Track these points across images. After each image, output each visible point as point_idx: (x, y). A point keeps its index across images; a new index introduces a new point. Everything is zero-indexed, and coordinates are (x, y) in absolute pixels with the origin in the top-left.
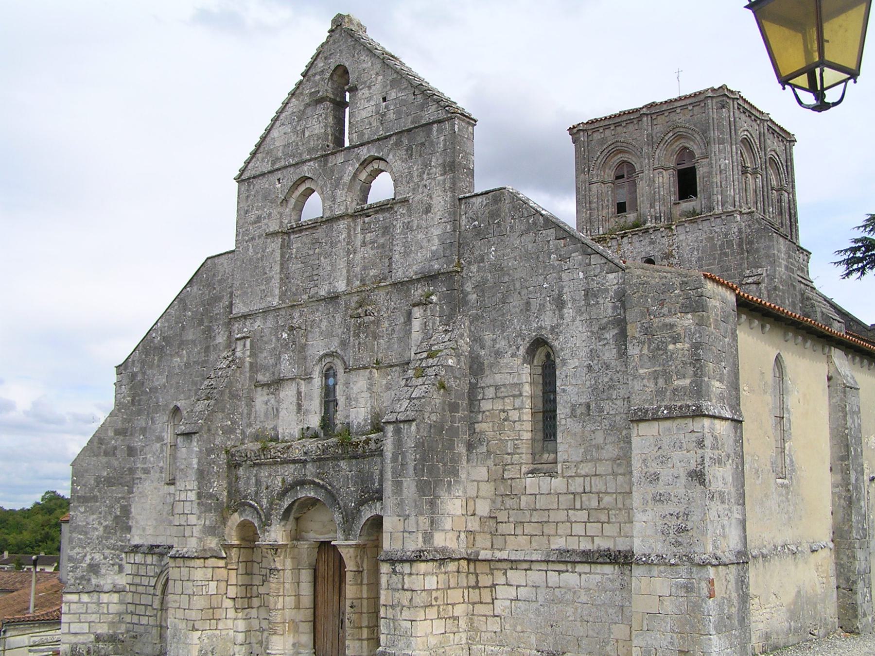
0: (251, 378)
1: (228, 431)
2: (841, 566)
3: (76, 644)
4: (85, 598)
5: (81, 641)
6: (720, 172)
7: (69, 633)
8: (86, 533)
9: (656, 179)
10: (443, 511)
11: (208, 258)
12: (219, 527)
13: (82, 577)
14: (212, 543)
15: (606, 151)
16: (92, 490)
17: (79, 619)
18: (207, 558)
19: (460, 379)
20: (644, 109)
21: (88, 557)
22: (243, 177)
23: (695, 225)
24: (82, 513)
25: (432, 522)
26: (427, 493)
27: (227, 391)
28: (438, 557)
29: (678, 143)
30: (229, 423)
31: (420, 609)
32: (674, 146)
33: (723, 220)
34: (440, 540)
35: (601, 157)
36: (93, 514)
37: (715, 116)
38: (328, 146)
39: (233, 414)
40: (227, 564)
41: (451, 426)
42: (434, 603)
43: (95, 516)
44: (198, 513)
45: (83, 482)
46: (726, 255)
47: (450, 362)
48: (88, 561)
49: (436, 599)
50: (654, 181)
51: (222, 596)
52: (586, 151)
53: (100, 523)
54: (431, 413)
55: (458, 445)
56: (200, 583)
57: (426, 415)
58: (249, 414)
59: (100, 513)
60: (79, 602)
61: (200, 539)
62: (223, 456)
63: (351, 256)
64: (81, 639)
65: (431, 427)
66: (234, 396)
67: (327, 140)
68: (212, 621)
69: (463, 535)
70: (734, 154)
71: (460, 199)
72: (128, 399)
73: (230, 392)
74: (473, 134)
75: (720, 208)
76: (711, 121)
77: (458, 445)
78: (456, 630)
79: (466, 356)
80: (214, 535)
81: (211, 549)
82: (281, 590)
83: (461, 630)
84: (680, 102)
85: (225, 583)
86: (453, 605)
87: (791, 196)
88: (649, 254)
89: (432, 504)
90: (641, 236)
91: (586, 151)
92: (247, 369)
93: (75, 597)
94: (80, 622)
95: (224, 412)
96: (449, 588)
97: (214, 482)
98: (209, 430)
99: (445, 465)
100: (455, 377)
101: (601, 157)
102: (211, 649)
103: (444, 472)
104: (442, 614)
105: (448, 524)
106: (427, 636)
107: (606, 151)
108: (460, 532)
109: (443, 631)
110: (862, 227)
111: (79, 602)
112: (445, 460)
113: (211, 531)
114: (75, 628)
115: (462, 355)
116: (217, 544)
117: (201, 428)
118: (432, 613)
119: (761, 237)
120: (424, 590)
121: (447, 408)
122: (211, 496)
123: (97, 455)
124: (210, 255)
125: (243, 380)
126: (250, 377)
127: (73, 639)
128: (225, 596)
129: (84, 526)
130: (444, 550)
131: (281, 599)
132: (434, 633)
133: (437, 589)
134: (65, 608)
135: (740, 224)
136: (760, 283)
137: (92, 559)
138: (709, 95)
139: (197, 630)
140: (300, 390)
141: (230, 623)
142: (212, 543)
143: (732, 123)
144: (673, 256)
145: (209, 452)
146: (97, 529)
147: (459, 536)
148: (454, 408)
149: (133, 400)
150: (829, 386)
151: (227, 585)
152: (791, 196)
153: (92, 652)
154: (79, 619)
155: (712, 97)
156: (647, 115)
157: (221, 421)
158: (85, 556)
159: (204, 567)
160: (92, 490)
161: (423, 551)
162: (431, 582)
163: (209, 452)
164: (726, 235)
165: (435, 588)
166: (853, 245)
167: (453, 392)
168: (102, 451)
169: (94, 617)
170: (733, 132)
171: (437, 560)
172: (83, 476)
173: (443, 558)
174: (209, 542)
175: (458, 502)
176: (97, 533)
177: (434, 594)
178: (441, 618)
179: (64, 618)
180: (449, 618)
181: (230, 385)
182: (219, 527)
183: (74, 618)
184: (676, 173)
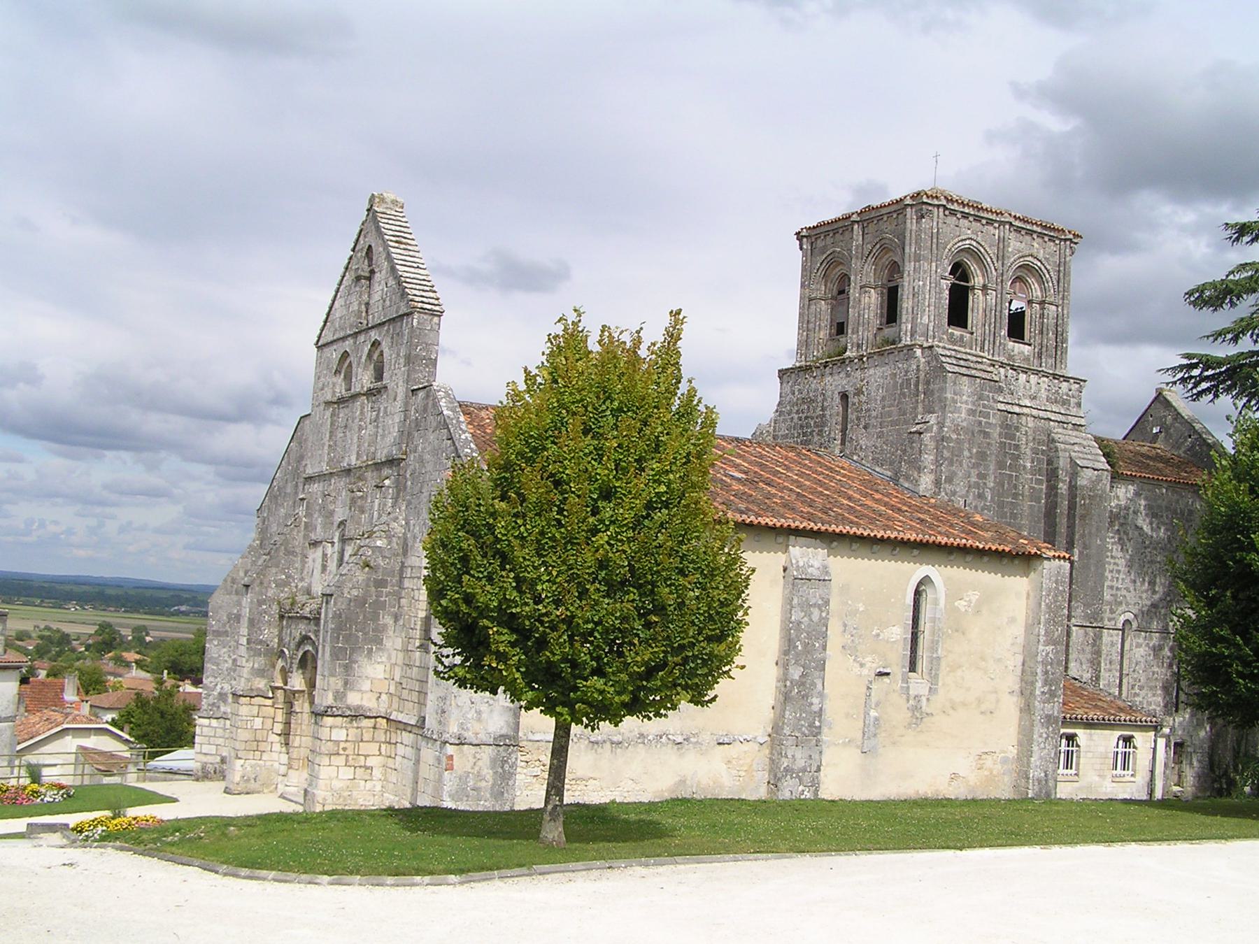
0: (306, 536)
1: (280, 584)
2: (773, 760)
3: (206, 763)
4: (214, 723)
5: (210, 761)
6: (914, 295)
7: (201, 753)
8: (218, 665)
9: (863, 299)
10: (360, 674)
11: (301, 418)
12: (268, 670)
13: (214, 704)
14: (261, 684)
15: (826, 262)
16: (224, 625)
17: (209, 741)
18: (253, 697)
19: (390, 558)
20: (854, 216)
21: (219, 687)
22: (319, 344)
23: (883, 358)
24: (215, 646)
25: (346, 683)
26: (341, 657)
27: (283, 548)
28: (348, 713)
29: (886, 257)
30: (284, 577)
31: (325, 756)
32: (884, 260)
33: (895, 356)
34: (353, 699)
35: (821, 269)
36: (224, 647)
37: (914, 228)
38: (361, 323)
39: (288, 568)
40: (274, 703)
41: (376, 600)
42: (341, 752)
43: (225, 650)
44: (246, 656)
45: (217, 618)
46: (904, 395)
47: (379, 543)
48: (219, 690)
49: (344, 749)
50: (860, 301)
51: (268, 731)
52: (809, 261)
53: (230, 657)
54: (351, 589)
55: (383, 617)
56: (245, 718)
57: (346, 591)
58: (302, 570)
59: (230, 647)
60: (209, 726)
61: (248, 680)
62: (275, 607)
63: (363, 432)
64: (209, 759)
65: (350, 601)
66: (289, 553)
67: (360, 318)
68: (256, 752)
69: (384, 697)
70: (933, 272)
71: (413, 391)
72: (257, 542)
73: (285, 549)
74: (439, 324)
75: (908, 339)
76: (908, 234)
77: (383, 617)
78: (367, 777)
79: (399, 537)
80: (263, 676)
81: (258, 689)
82: (299, 730)
83: (374, 778)
84: (886, 209)
85: (272, 720)
86: (366, 756)
87: (1060, 309)
88: (844, 388)
89: (348, 668)
90: (840, 367)
91: (809, 261)
92: (303, 529)
93: (206, 722)
94: (209, 744)
95: (278, 567)
96: (362, 741)
97: (265, 630)
98: (261, 583)
99: (365, 634)
100: (384, 557)
101: (821, 269)
102: (254, 776)
103: (364, 640)
104: (351, 762)
105: (366, 686)
106: (331, 779)
107: (826, 262)
108: (380, 693)
109: (352, 777)
110: (1211, 336)
111: (209, 726)
112: (367, 630)
113: (260, 673)
114: (206, 749)
115: (394, 536)
116: (266, 685)
117: (253, 581)
118: (340, 760)
119: (936, 377)
120: (330, 740)
121: (372, 584)
122: (261, 642)
123: (230, 594)
124: (303, 415)
125: (298, 539)
126: (305, 535)
127: (205, 759)
128: (270, 732)
129: (216, 658)
130: (359, 707)
131: (298, 738)
132: (340, 777)
133: (347, 741)
134: (198, 730)
135: (919, 361)
136: (922, 433)
137: (222, 688)
138: (907, 203)
139: (240, 758)
140: (326, 552)
141: (275, 756)
142: (261, 684)
143: (935, 236)
144: (863, 393)
145: (260, 603)
146: (226, 661)
147: (380, 697)
148: (380, 584)
149: (261, 544)
150: (784, 577)
151: (274, 722)
152: (1060, 309)
153: (218, 771)
154: (209, 741)
155: (912, 206)
156: (858, 222)
157: (274, 574)
158: (217, 685)
159: (250, 704)
160: (224, 625)
161: (332, 707)
162: (339, 735)
163: (260, 603)
164: (907, 372)
165: (344, 739)
166: (1185, 362)
167: (381, 570)
168: (234, 589)
169: (220, 741)
170: (934, 246)
171: (347, 717)
172: (217, 612)
173: (356, 715)
174: (256, 683)
175: (380, 668)
176: (226, 665)
177: (342, 745)
178: (350, 766)
179: (197, 739)
180: (360, 767)
181: (286, 542)
182: (268, 670)
183: (205, 740)
184: (885, 291)
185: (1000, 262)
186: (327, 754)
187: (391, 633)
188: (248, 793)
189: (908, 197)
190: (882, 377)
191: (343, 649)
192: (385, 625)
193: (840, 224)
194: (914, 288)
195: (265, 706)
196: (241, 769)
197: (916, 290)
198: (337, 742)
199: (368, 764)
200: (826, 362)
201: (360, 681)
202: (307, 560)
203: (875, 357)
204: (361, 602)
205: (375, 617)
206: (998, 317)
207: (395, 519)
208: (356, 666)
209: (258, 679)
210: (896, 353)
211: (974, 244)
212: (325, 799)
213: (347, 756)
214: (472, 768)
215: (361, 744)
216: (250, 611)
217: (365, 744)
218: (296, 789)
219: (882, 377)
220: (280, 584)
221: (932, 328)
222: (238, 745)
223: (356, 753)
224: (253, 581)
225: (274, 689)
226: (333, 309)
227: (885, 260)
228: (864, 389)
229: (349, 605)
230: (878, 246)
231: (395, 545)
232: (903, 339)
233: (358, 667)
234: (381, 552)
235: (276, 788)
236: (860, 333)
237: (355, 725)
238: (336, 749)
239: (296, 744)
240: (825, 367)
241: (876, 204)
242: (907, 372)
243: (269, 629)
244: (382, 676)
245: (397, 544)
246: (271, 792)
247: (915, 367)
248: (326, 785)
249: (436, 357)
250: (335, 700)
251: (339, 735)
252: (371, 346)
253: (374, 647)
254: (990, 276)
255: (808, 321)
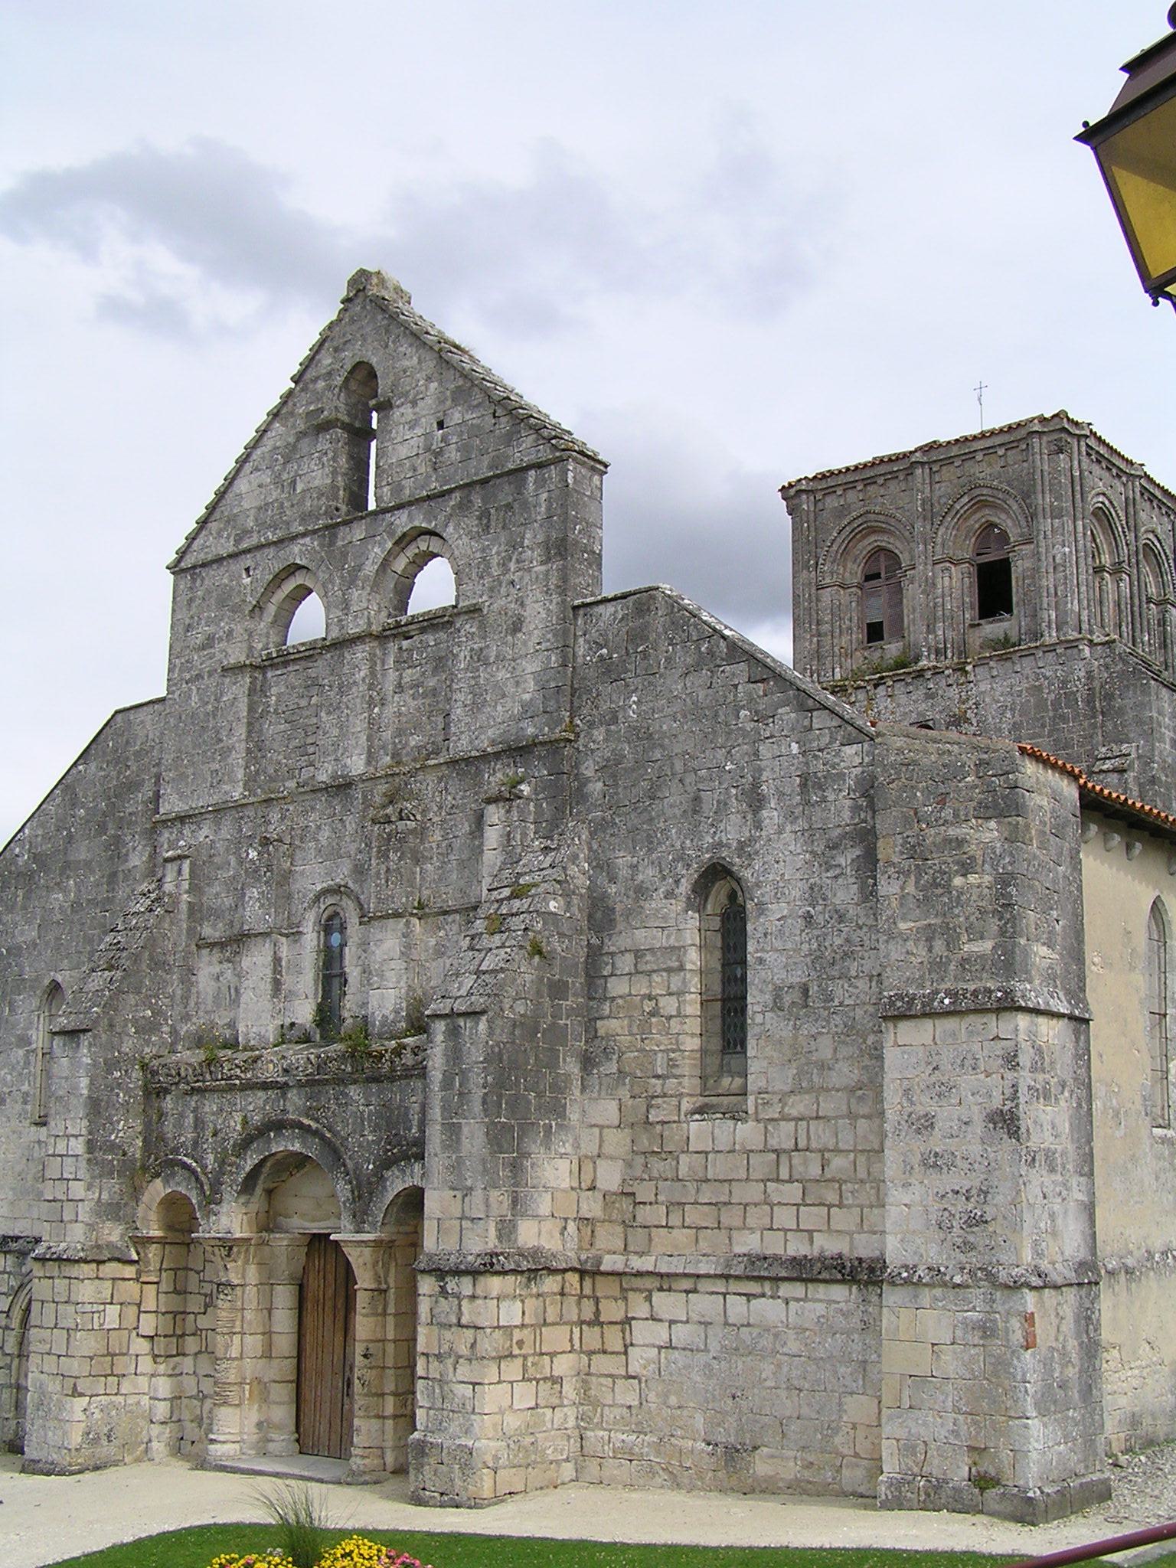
6: (1055, 568)
11: (117, 712)
12: (126, 1204)
19: (570, 937)
20: (917, 454)
25: (515, 1202)
26: (505, 1146)
28: (525, 1266)
29: (978, 515)
34: (528, 1234)
38: (337, 509)
39: (157, 996)
40: (139, 1273)
42: (516, 1351)
46: (1064, 718)
47: (553, 906)
49: (520, 1344)
51: (130, 1332)
52: (812, 529)
54: (515, 1000)
56: (88, 1308)
58: (186, 998)
61: (91, 1227)
62: (136, 1074)
63: (376, 710)
65: (514, 1026)
66: (157, 964)
71: (575, 608)
73: (151, 959)
76: (1038, 476)
77: (564, 1060)
79: (581, 895)
80: (117, 1219)
81: (110, 1245)
82: (238, 1323)
83: (566, 1402)
85: (135, 1308)
86: (552, 1355)
88: (924, 715)
89: (515, 1167)
91: (812, 529)
92: (184, 916)
96: (545, 1324)
97: (118, 1122)
98: (111, 1026)
100: (561, 935)
102: (105, 1430)
103: (539, 1108)
105: (544, 1206)
106: (501, 1412)
108: (566, 1220)
109: (532, 1404)
113: (111, 1211)
115: (574, 893)
116: (122, 1236)
117: (96, 1022)
118: (512, 1370)
120: (498, 1327)
121: (545, 990)
122: (112, 1147)
125: (176, 935)
126: (189, 929)
128: (134, 1333)
130: (536, 1253)
131: (237, 1339)
132: (515, 1407)
133: (523, 1325)
136: (1125, 771)
138: (1036, 429)
139: (81, 1395)
141: (143, 1382)
142: (113, 1234)
144: (967, 721)
145: (111, 1065)
148: (558, 990)
151: (140, 1312)
156: (922, 464)
159: (97, 1278)
161: (497, 1255)
162: (511, 1313)
163: (111, 1065)
167: (558, 962)
171: (522, 1272)
174: (106, 1231)
175: (564, 1165)
177: (517, 1335)
180: (545, 1379)
181: (151, 943)
182: (126, 1204)
185: (1133, 535)
186: (493, 1358)
187: (577, 1092)
188: (97, 1468)
189: (1036, 421)
190: (1010, 694)
191: (507, 1128)
192: (568, 1076)
193: (882, 469)
194: (1054, 557)
195: (124, 1279)
196: (83, 1418)
197: (1058, 560)
198: (508, 1329)
199: (555, 1373)
200: (882, 678)
201: (536, 1195)
202: (194, 978)
203: (992, 664)
204: (529, 1027)
205: (553, 1064)
206: (1137, 614)
207: (574, 858)
208: (528, 1164)
209: (108, 1224)
210: (1041, 654)
211: (1107, 503)
212: (496, 1458)
213: (525, 1357)
214: (1057, 1340)
215: (543, 1329)
216: (91, 1083)
217: (550, 1328)
218: (237, 1446)
219: (1010, 694)
220: (146, 1029)
221: (1086, 618)
222: (74, 1366)
223: (538, 1350)
224: (96, 1022)
225: (141, 1242)
226: (230, 496)
227: (976, 521)
228: (969, 714)
229: (513, 1033)
230: (966, 499)
231: (575, 909)
232: (1046, 633)
233: (533, 1165)
234: (556, 924)
235: (146, 1450)
236: (940, 632)
237: (535, 1290)
238: (508, 1344)
239: (234, 1352)
240: (876, 686)
241: (943, 439)
242: (1065, 683)
243: (126, 1121)
244: (565, 1184)
245: (580, 910)
246: (138, 1460)
247: (1082, 674)
248: (495, 1425)
249: (601, 550)
250: (500, 1238)
251: (511, 1313)
252: (396, 543)
253: (554, 1123)
254: (1121, 551)
255: (818, 621)
